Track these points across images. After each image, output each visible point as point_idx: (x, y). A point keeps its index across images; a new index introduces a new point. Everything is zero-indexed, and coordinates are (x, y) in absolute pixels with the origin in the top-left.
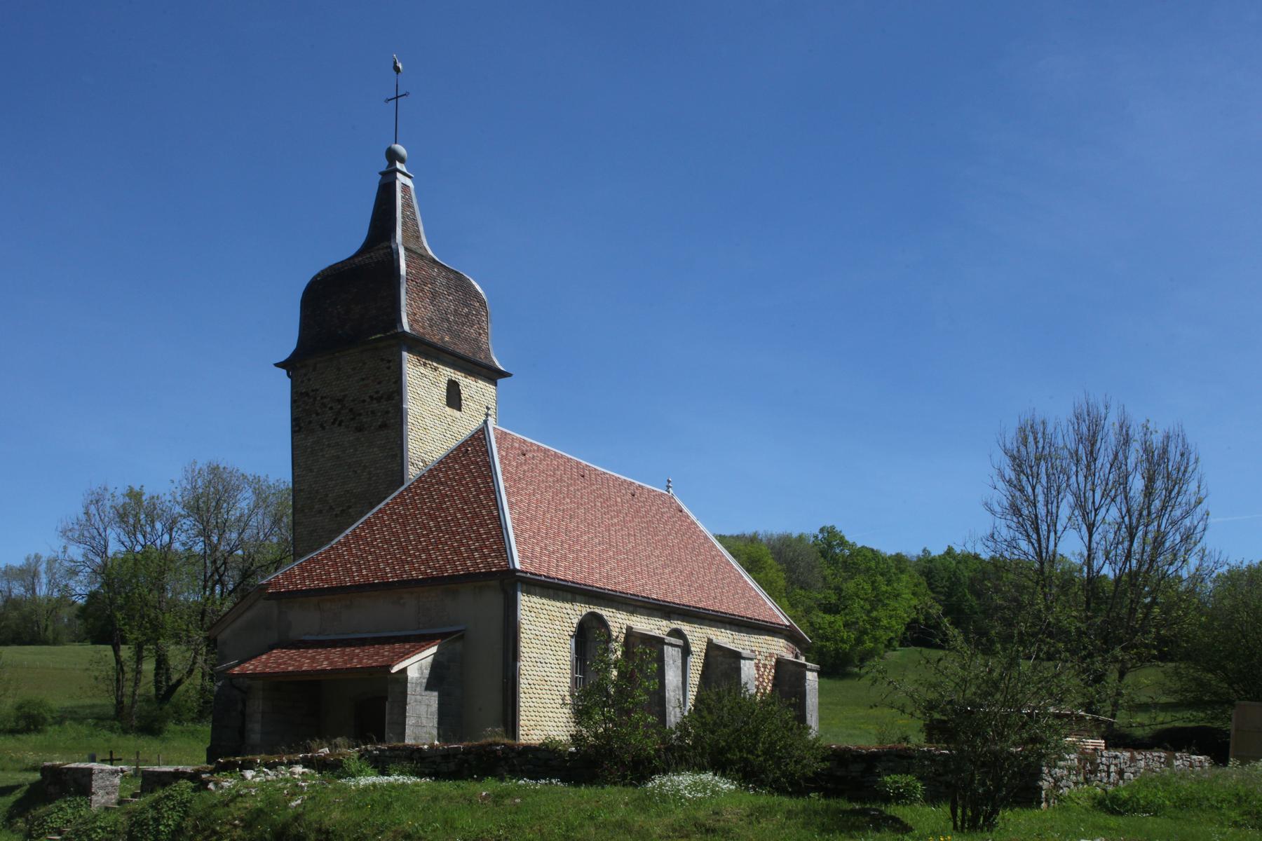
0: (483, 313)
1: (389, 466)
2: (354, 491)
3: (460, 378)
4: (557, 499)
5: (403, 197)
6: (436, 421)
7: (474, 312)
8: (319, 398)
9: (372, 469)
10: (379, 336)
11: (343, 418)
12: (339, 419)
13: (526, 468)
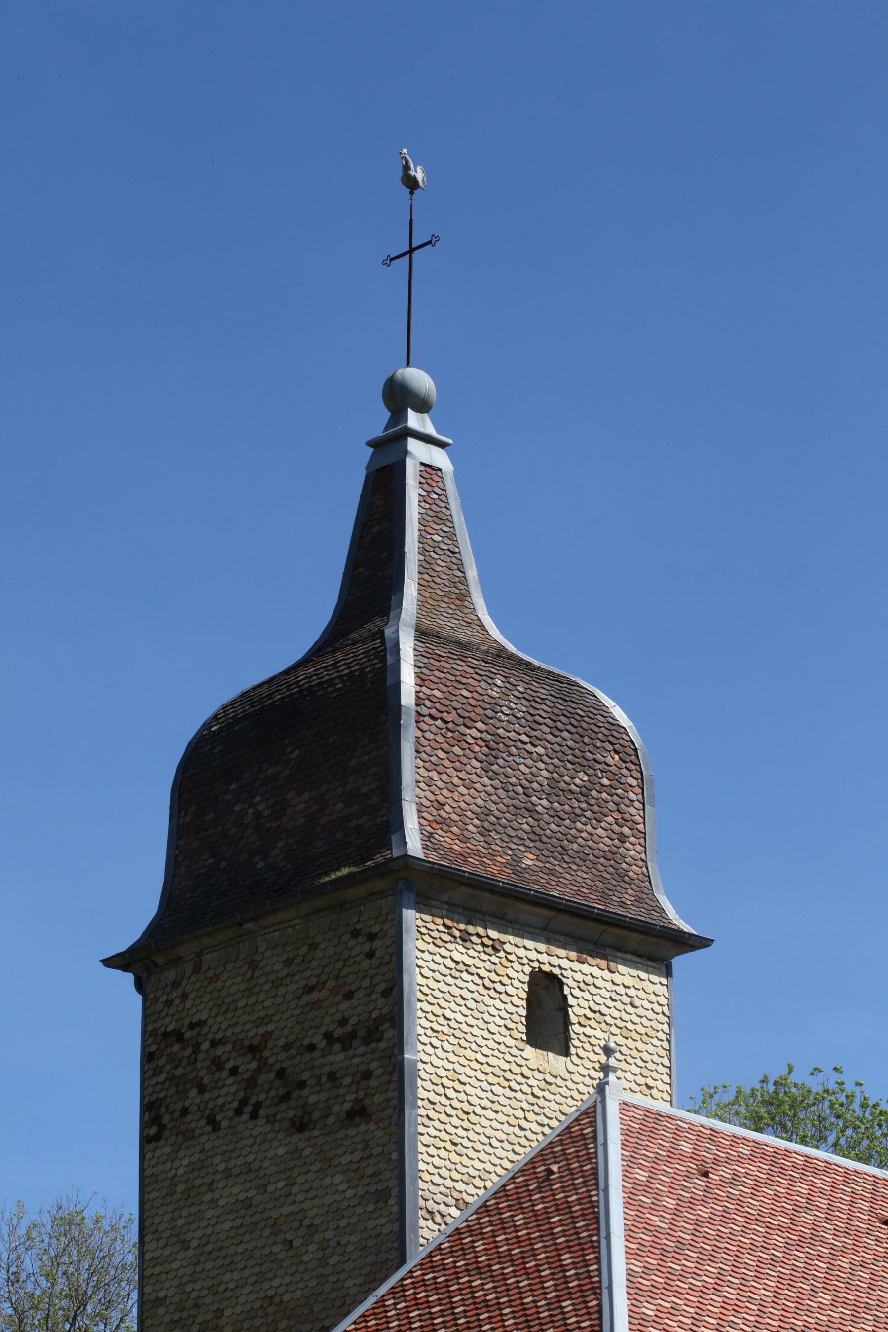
0: (630, 780)
1: (371, 1224)
2: (286, 1298)
3: (565, 963)
4: (788, 1298)
5: (423, 499)
6: (497, 1089)
7: (605, 782)
8: (205, 1046)
9: (329, 1235)
10: (345, 871)
11: (262, 1097)
12: (253, 1100)
13: (704, 1212)
